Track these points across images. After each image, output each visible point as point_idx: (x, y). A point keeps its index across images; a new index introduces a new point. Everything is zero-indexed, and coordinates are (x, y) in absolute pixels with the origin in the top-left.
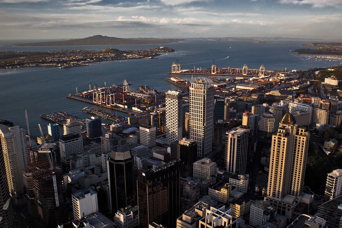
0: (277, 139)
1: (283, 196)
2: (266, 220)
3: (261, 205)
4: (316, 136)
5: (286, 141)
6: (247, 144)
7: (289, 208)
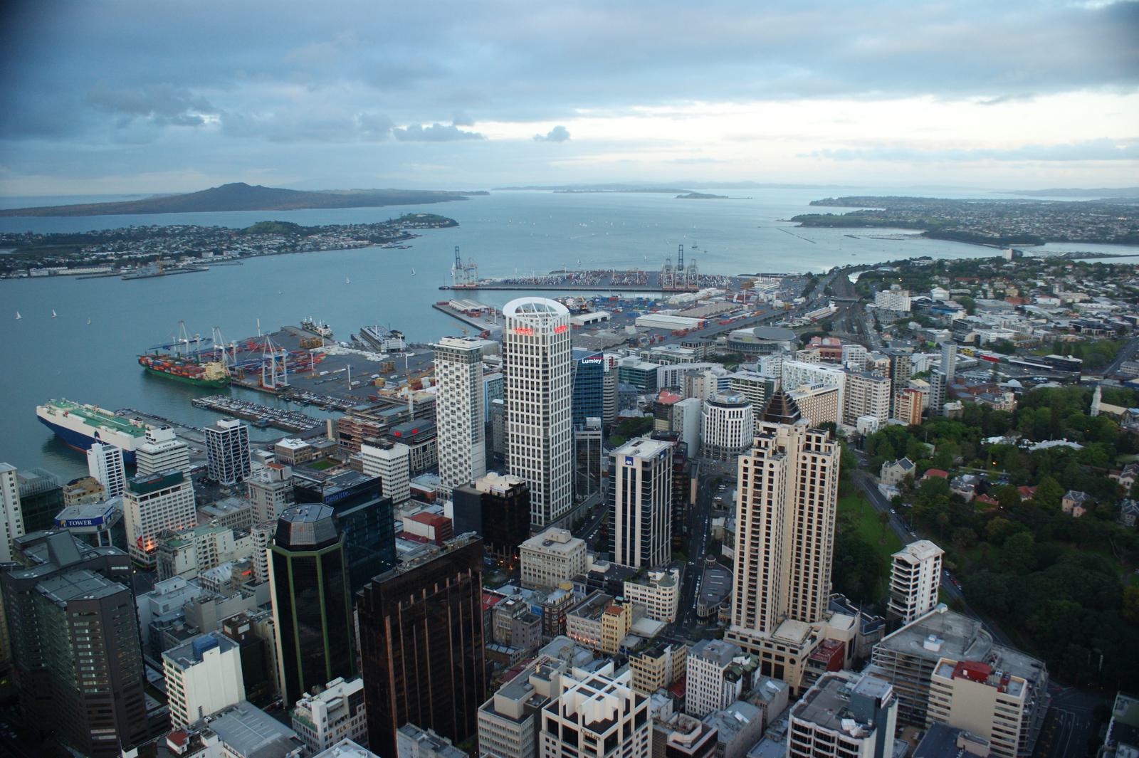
0: (751, 466)
7: (793, 656)
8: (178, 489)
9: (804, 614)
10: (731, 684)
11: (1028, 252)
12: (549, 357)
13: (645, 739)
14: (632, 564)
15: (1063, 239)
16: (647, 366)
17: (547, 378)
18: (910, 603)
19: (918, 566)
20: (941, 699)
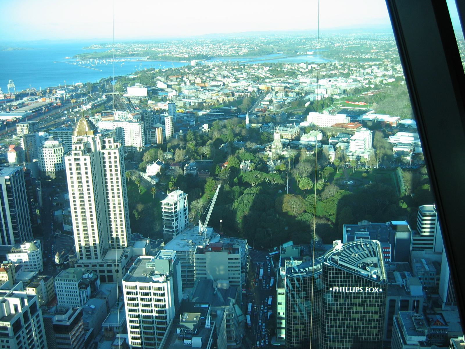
0: (74, 163)
1: (104, 252)
2: (85, 297)
3: (71, 276)
4: (132, 162)
5: (88, 161)
6: (28, 219)
10: (84, 291)
13: (42, 342)
18: (174, 225)
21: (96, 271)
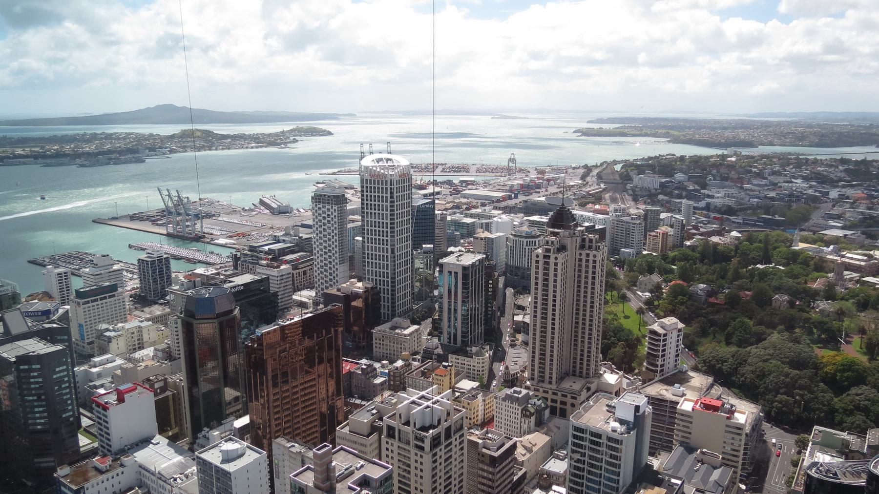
7: (573, 401)
8: (113, 296)
9: (581, 373)
11: (745, 152)
12: (395, 195)
14: (455, 343)
15: (771, 144)
16: (468, 220)
17: (393, 211)
19: (665, 335)
20: (684, 426)
21: (547, 399)
